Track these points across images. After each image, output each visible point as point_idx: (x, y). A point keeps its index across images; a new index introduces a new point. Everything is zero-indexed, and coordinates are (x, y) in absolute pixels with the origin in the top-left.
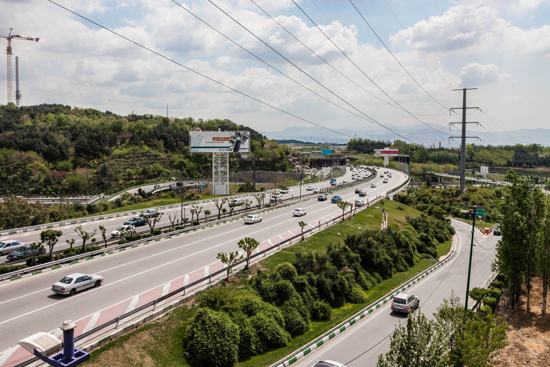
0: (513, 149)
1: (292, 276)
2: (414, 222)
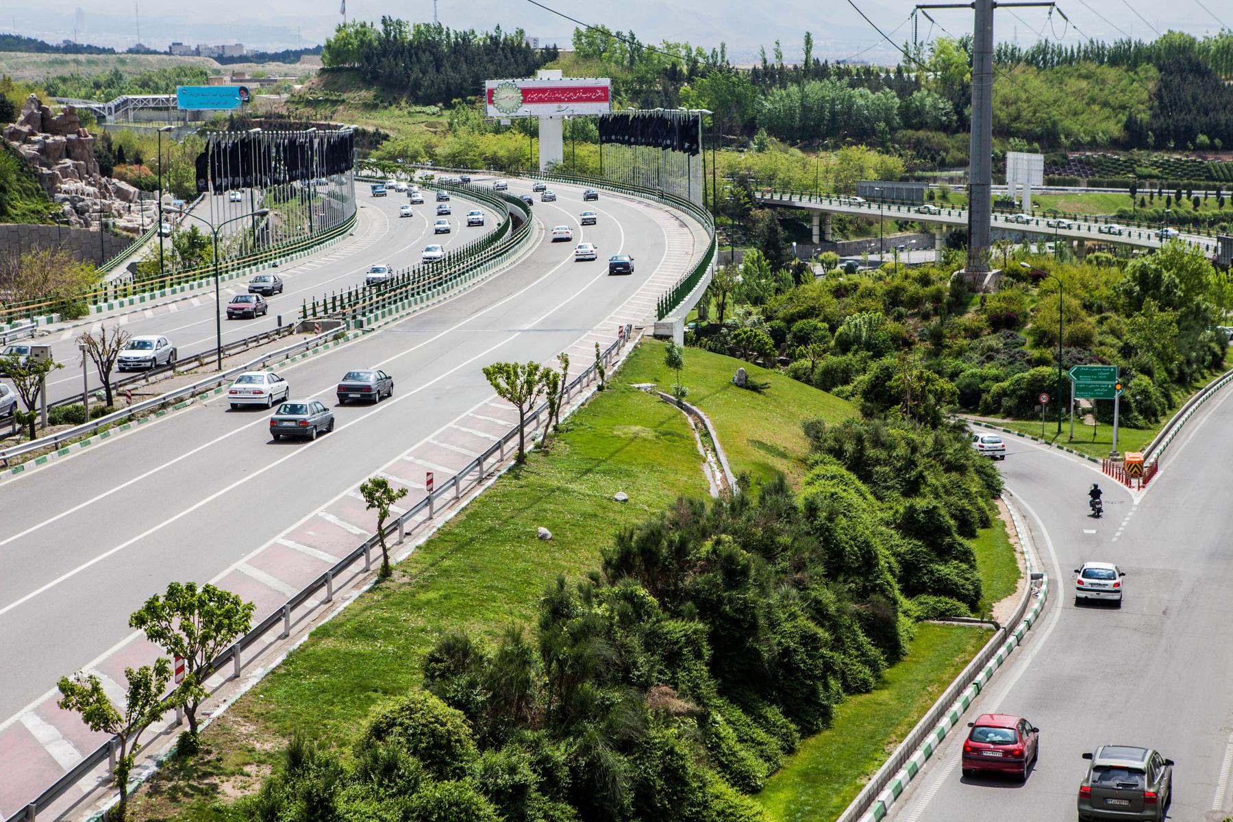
0: (1149, 59)
1: (455, 757)
2: (849, 447)
